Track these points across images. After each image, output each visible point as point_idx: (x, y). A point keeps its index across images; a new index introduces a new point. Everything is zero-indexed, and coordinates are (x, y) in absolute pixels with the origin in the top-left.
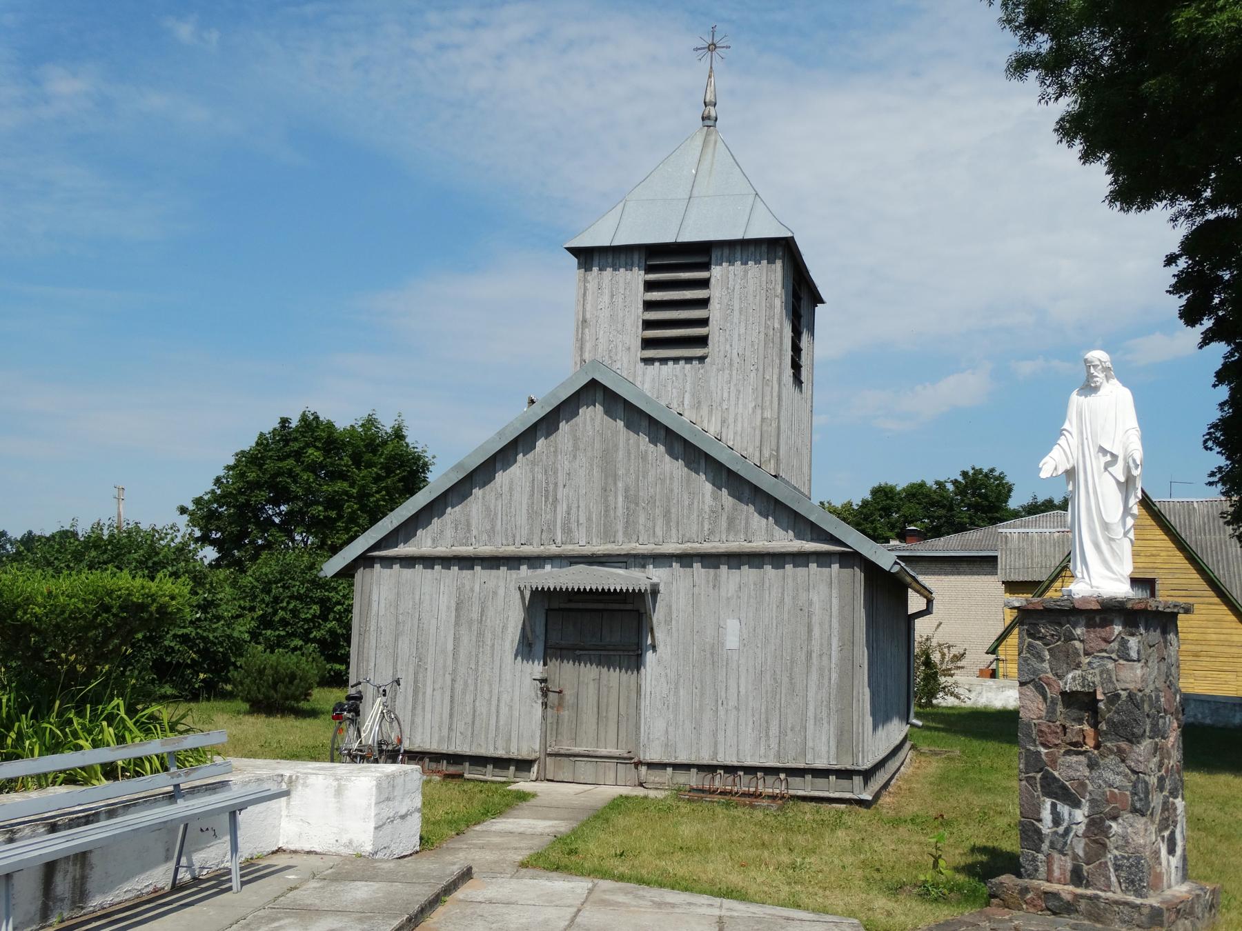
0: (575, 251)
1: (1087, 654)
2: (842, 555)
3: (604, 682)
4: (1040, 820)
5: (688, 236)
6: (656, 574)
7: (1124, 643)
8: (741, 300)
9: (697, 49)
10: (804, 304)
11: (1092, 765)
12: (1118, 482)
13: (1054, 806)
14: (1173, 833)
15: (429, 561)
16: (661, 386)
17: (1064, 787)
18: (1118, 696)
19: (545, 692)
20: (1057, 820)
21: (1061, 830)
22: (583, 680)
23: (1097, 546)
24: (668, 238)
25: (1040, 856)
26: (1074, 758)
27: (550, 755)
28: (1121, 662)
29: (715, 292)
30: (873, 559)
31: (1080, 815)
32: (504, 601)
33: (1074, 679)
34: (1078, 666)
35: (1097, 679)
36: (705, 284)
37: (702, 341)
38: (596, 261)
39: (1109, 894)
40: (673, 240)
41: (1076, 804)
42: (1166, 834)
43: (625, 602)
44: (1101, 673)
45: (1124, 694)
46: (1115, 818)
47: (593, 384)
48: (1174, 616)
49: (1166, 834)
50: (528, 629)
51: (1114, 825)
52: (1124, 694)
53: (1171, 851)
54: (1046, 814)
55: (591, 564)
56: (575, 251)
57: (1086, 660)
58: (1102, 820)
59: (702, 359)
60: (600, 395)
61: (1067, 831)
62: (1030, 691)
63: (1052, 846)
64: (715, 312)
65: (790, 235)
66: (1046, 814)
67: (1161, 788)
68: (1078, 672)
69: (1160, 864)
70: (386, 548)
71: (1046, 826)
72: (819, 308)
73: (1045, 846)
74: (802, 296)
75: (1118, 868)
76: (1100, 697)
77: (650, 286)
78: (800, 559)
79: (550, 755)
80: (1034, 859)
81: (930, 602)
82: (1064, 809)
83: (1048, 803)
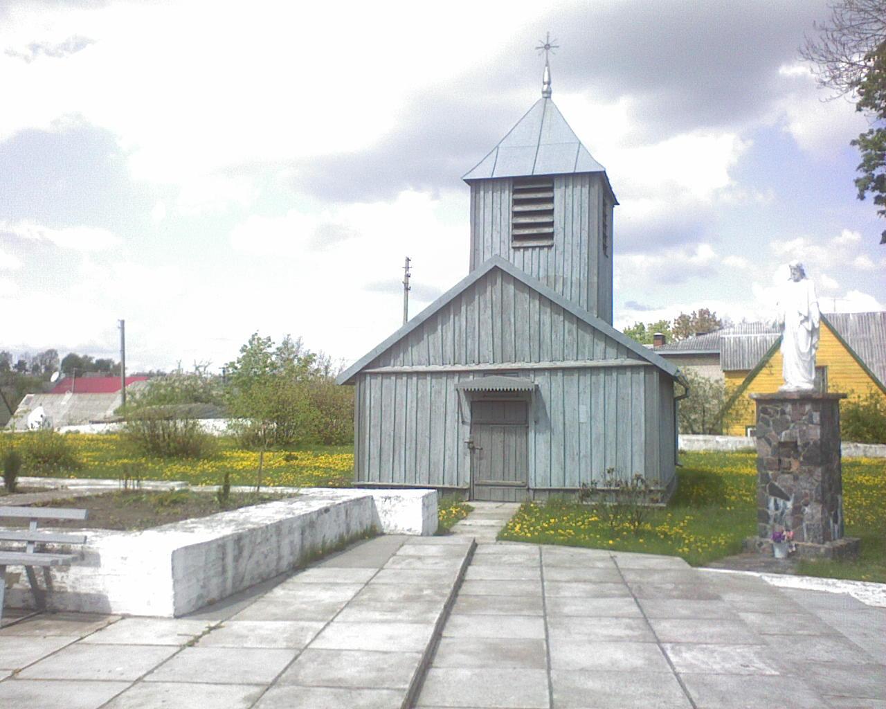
0: (469, 182)
1: (793, 422)
2: (645, 367)
3: (507, 442)
4: (768, 508)
5: (540, 171)
6: (539, 380)
7: (811, 416)
8: (569, 208)
9: (538, 48)
10: (608, 206)
11: (796, 478)
12: (808, 331)
13: (775, 501)
14: (836, 512)
15: (398, 374)
16: (525, 263)
17: (780, 490)
18: (809, 443)
19: (473, 449)
20: (777, 508)
21: (778, 513)
22: (493, 441)
23: (834, 532)
24: (527, 172)
25: (768, 526)
26: (786, 476)
27: (476, 485)
28: (810, 425)
29: (557, 205)
30: (664, 369)
31: (790, 504)
32: (448, 397)
33: (786, 434)
34: (788, 428)
35: (798, 435)
36: (551, 200)
37: (550, 236)
38: (482, 188)
39: (804, 543)
40: (530, 174)
41: (788, 499)
42: (833, 513)
43: (517, 396)
44: (800, 431)
45: (812, 443)
46: (806, 505)
47: (496, 269)
48: (837, 401)
49: (833, 513)
50: (208, 414)
51: (806, 509)
52: (812, 443)
53: (835, 522)
54: (772, 505)
55: (497, 374)
56: (469, 182)
57: (792, 425)
58: (800, 507)
59: (550, 247)
60: (499, 274)
61: (782, 513)
62: (763, 442)
63: (775, 521)
64: (558, 217)
65: (603, 170)
66: (772, 505)
67: (830, 489)
68: (788, 431)
69: (829, 527)
70: (369, 368)
71: (771, 511)
72: (616, 208)
73: (771, 522)
74: (609, 199)
75: (808, 530)
76: (799, 443)
77: (517, 202)
78: (621, 369)
79: (476, 485)
80: (765, 528)
81: (687, 389)
82: (781, 502)
83: (772, 500)
